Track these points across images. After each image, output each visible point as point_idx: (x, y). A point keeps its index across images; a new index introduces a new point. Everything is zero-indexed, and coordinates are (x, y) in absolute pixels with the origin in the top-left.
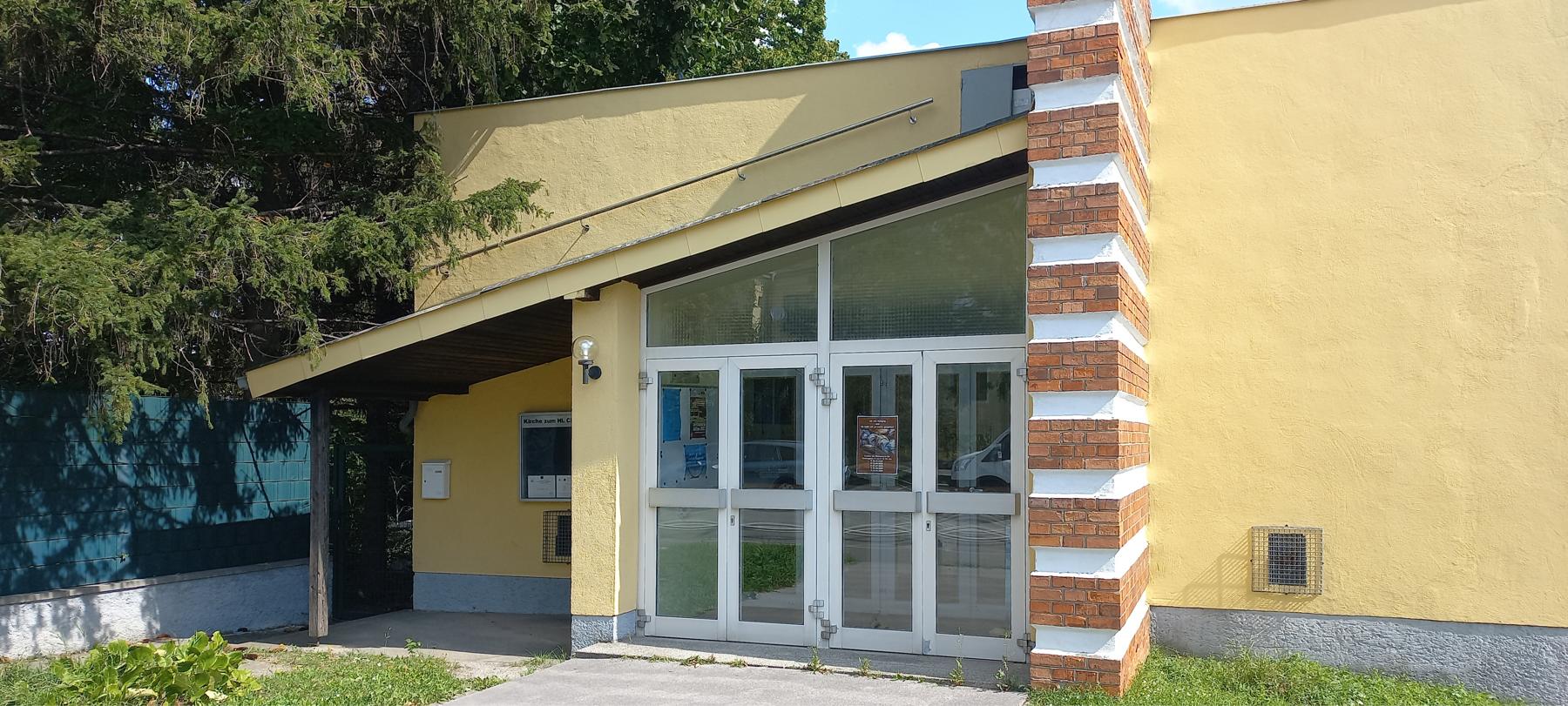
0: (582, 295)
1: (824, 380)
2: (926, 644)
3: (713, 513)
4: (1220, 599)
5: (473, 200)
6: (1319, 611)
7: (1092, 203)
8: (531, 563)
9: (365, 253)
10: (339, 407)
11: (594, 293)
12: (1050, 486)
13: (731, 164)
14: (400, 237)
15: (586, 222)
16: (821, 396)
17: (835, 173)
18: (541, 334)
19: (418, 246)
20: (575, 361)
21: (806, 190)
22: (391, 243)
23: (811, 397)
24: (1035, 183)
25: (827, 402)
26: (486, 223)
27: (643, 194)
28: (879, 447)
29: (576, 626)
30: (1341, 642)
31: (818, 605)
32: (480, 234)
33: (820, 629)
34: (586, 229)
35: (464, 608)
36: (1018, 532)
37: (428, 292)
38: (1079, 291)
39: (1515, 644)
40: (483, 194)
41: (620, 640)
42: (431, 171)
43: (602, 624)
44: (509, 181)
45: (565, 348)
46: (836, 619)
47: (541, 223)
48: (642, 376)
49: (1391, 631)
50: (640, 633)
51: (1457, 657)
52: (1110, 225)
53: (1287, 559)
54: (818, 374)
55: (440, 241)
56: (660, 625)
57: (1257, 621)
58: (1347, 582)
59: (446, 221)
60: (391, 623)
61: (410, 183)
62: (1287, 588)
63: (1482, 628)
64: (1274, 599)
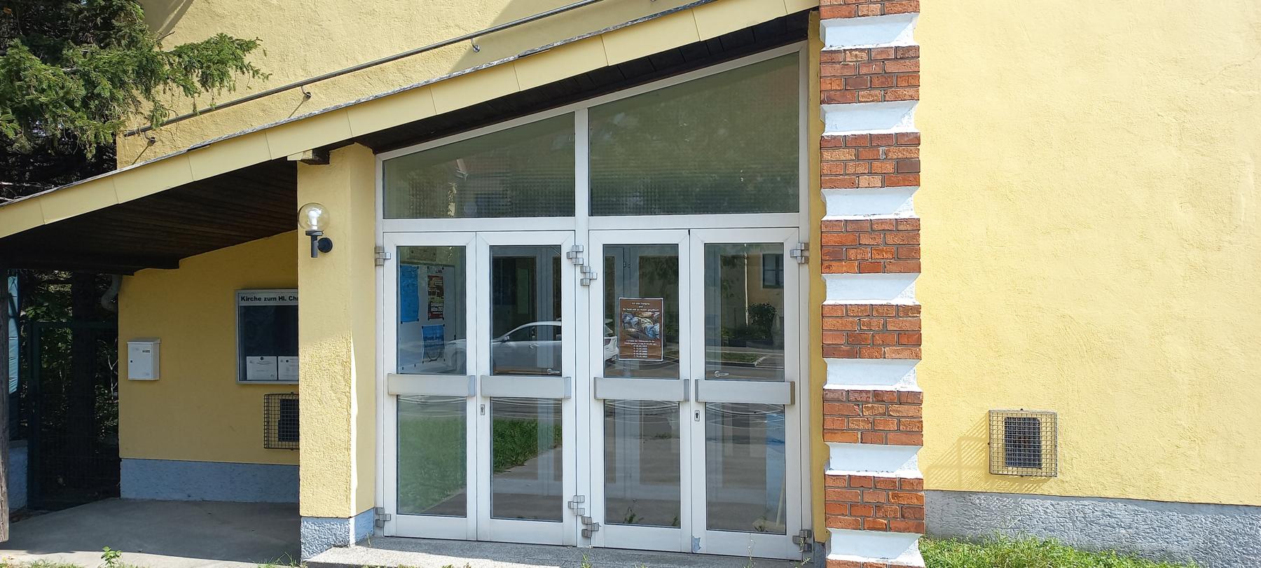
0: (310, 156)
1: (583, 258)
2: (695, 541)
3: (461, 405)
4: (960, 481)
5: (179, 52)
6: (1053, 493)
7: (891, 67)
8: (247, 443)
9: (43, 99)
10: (53, 282)
11: (323, 155)
12: (847, 376)
13: (462, 34)
14: (90, 84)
15: (307, 88)
16: (580, 276)
17: (602, 28)
18: (257, 203)
19: (113, 98)
20: (301, 231)
21: (568, 45)
22: (78, 89)
23: (569, 275)
24: (828, 44)
25: (586, 283)
26: (195, 79)
27: (369, 61)
28: (643, 331)
29: (306, 529)
30: (1074, 522)
31: (578, 500)
32: (188, 90)
33: (581, 527)
34: (308, 96)
35: (176, 497)
36: (796, 427)
37: (128, 150)
38: (876, 164)
39: (1232, 523)
40: (193, 47)
41: (357, 544)
42: (133, 22)
43: (337, 527)
44: (222, 37)
45: (288, 219)
46: (598, 515)
47: (258, 86)
48: (378, 251)
49: (1121, 512)
50: (379, 533)
51: (1183, 537)
52: (911, 91)
53: (1023, 442)
54: (576, 251)
55: (141, 98)
56: (400, 524)
57: (995, 503)
58: (1086, 463)
59: (148, 73)
60: (91, 518)
61: (109, 36)
62: (1024, 471)
63: (1204, 508)
64: (1012, 482)
